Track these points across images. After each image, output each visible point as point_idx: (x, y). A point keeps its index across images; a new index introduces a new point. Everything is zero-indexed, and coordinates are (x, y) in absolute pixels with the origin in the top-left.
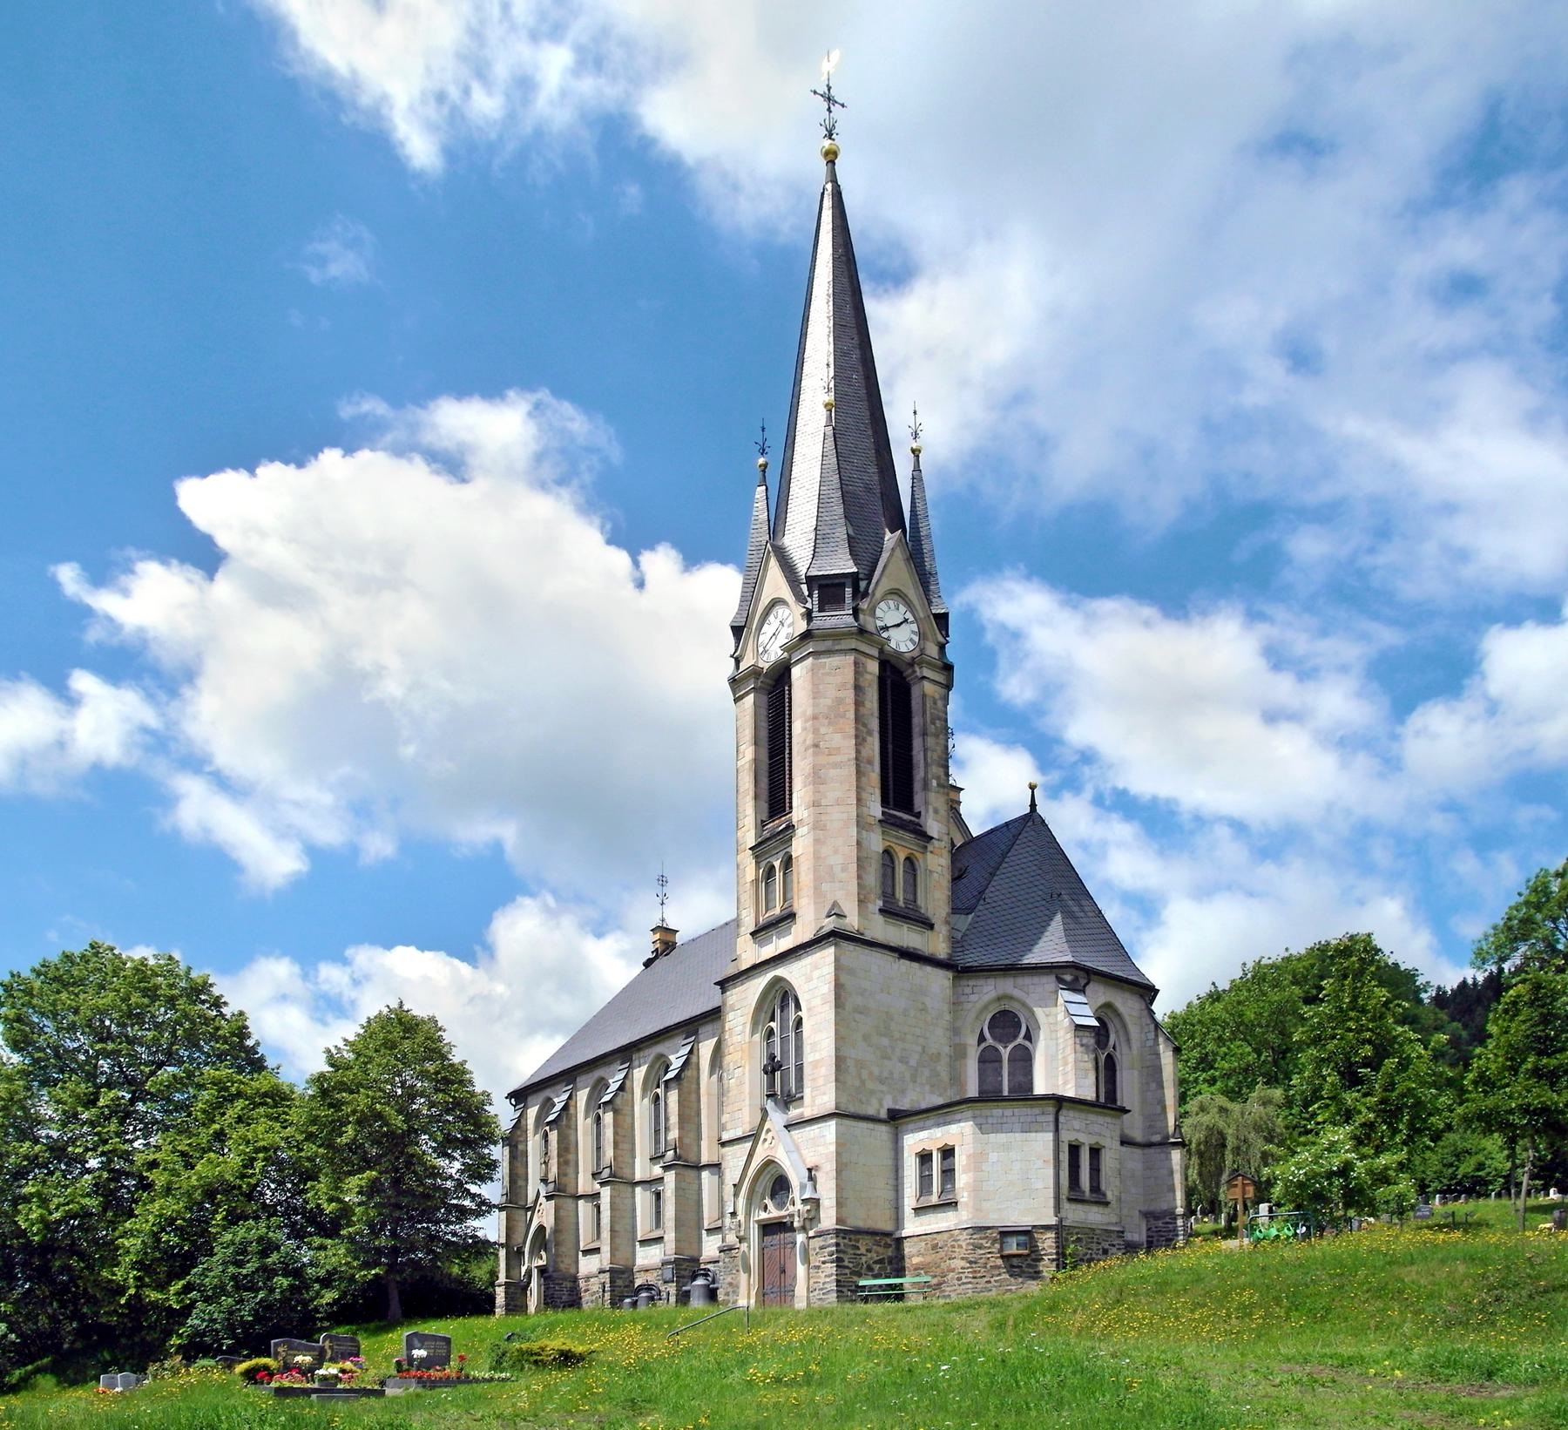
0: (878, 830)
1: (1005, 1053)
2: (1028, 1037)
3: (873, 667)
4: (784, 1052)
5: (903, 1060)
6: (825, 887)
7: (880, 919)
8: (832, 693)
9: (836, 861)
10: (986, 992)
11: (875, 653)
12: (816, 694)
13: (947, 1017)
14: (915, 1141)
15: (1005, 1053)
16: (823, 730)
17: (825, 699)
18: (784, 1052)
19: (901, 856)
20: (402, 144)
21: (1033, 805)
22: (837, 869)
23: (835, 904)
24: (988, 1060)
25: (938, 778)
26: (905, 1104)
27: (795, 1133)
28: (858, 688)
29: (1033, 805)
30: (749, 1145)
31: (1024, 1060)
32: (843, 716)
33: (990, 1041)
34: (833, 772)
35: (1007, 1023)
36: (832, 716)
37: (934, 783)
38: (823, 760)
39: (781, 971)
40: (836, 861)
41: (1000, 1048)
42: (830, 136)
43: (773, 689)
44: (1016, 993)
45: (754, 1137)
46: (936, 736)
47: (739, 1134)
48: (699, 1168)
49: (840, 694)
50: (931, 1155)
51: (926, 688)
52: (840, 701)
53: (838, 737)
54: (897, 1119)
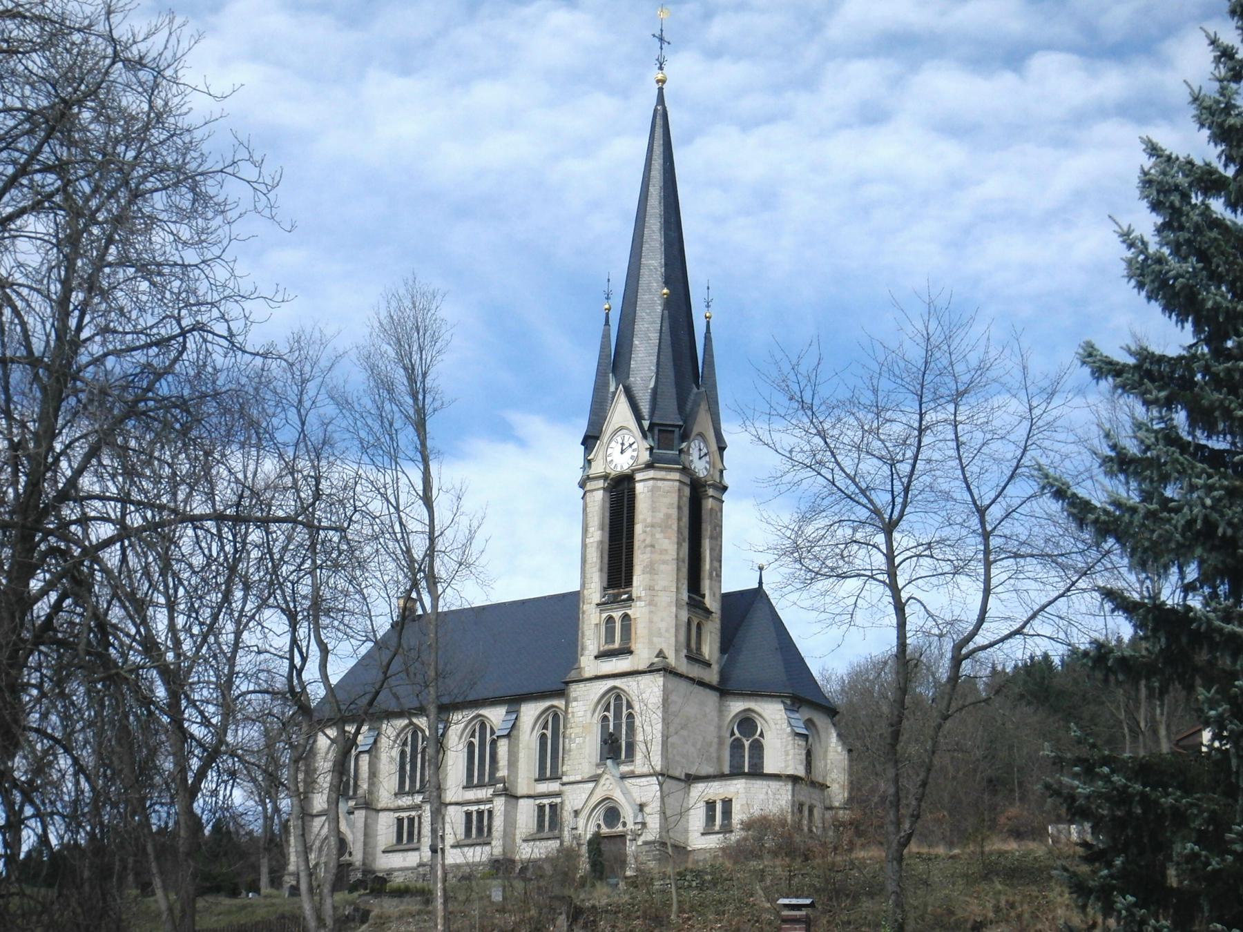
0: (686, 608)
1: (747, 744)
2: (762, 735)
4: (618, 726)
5: (694, 745)
6: (655, 640)
7: (685, 660)
8: (664, 510)
9: (663, 625)
10: (737, 706)
12: (654, 510)
14: (700, 791)
15: (747, 744)
16: (658, 536)
17: (656, 502)
18: (618, 726)
20: (601, 542)
21: (761, 583)
22: (663, 631)
24: (737, 746)
26: (692, 771)
27: (628, 782)
28: (679, 508)
29: (761, 583)
30: (591, 785)
31: (758, 748)
32: (670, 527)
33: (737, 734)
34: (663, 567)
35: (747, 723)
36: (664, 527)
38: (657, 557)
39: (617, 682)
40: (663, 625)
41: (744, 740)
42: (708, 306)
43: (621, 492)
45: (595, 779)
47: (579, 778)
48: (517, 798)
49: (670, 511)
50: (278, 889)
52: (668, 516)
53: (667, 541)
54: (691, 779)
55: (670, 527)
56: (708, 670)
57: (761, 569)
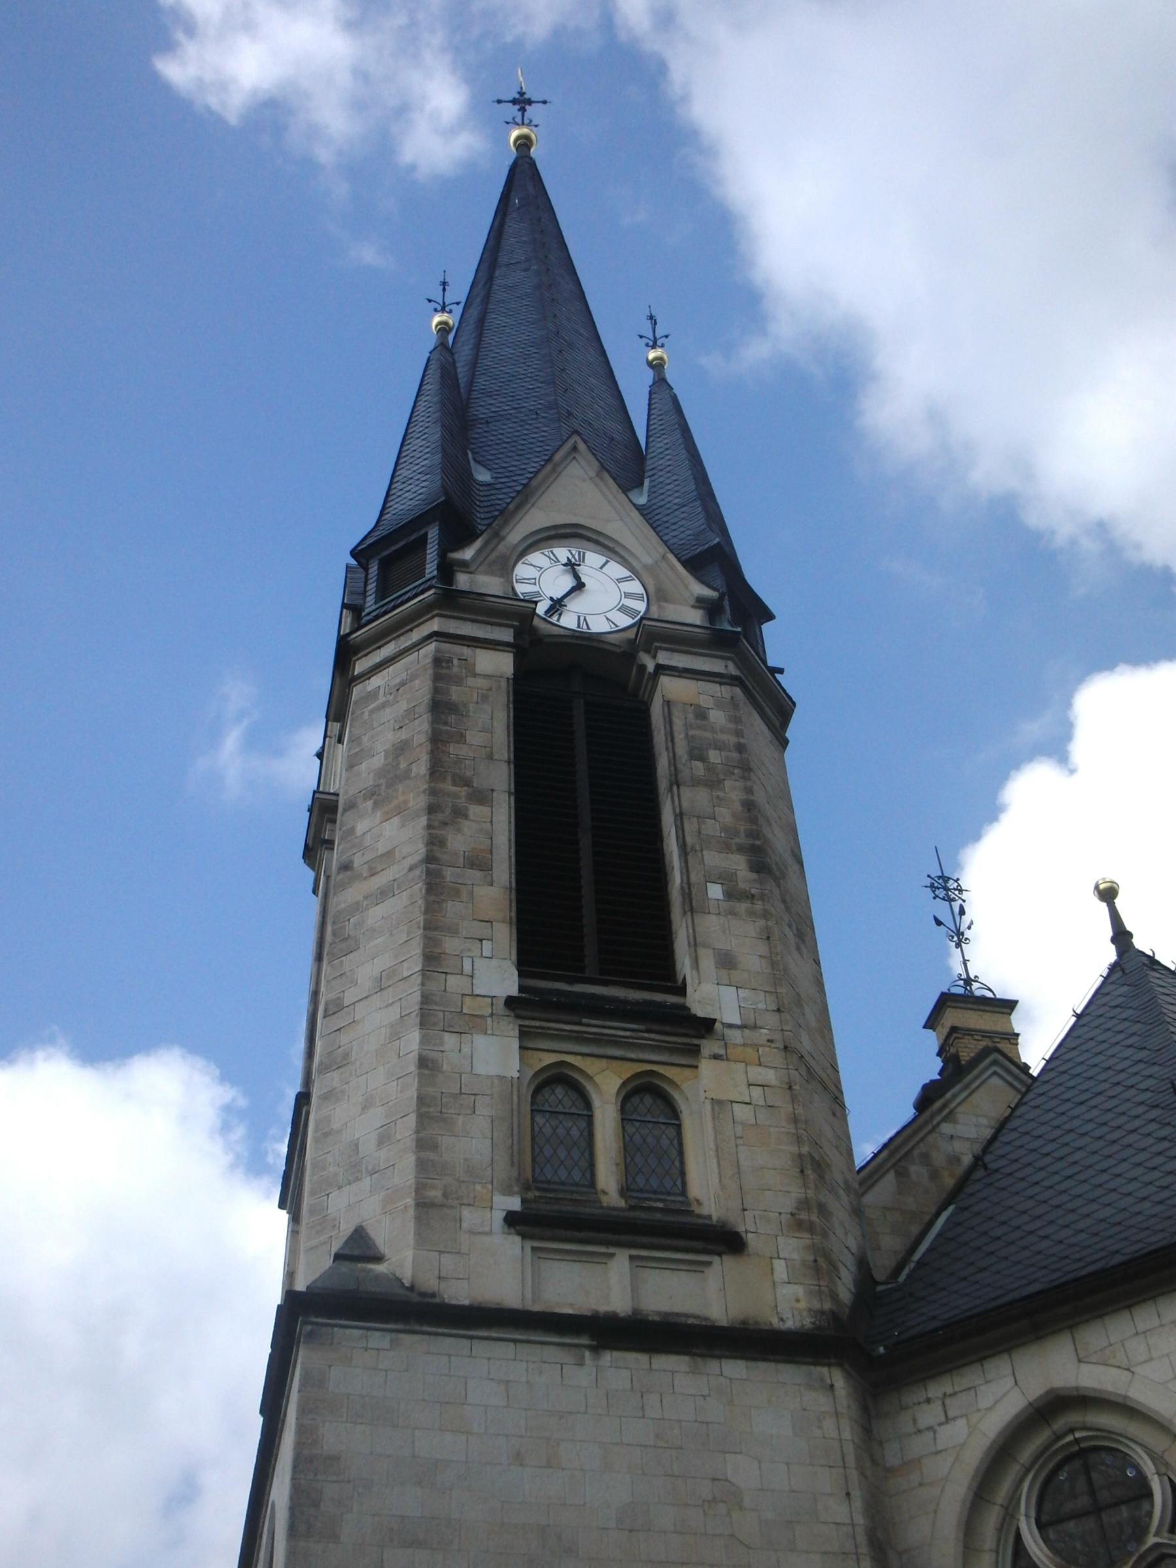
3: (501, 664)
7: (512, 1246)
11: (507, 635)
13: (839, 1511)
19: (606, 1084)
21: (1121, 937)
23: (359, 1235)
25: (726, 879)
29: (1121, 937)
32: (406, 775)
37: (715, 891)
44: (1091, 1378)
46: (712, 782)
49: (403, 735)
51: (687, 699)
55: (406, 775)
56: (721, 1268)
57: (1108, 895)
